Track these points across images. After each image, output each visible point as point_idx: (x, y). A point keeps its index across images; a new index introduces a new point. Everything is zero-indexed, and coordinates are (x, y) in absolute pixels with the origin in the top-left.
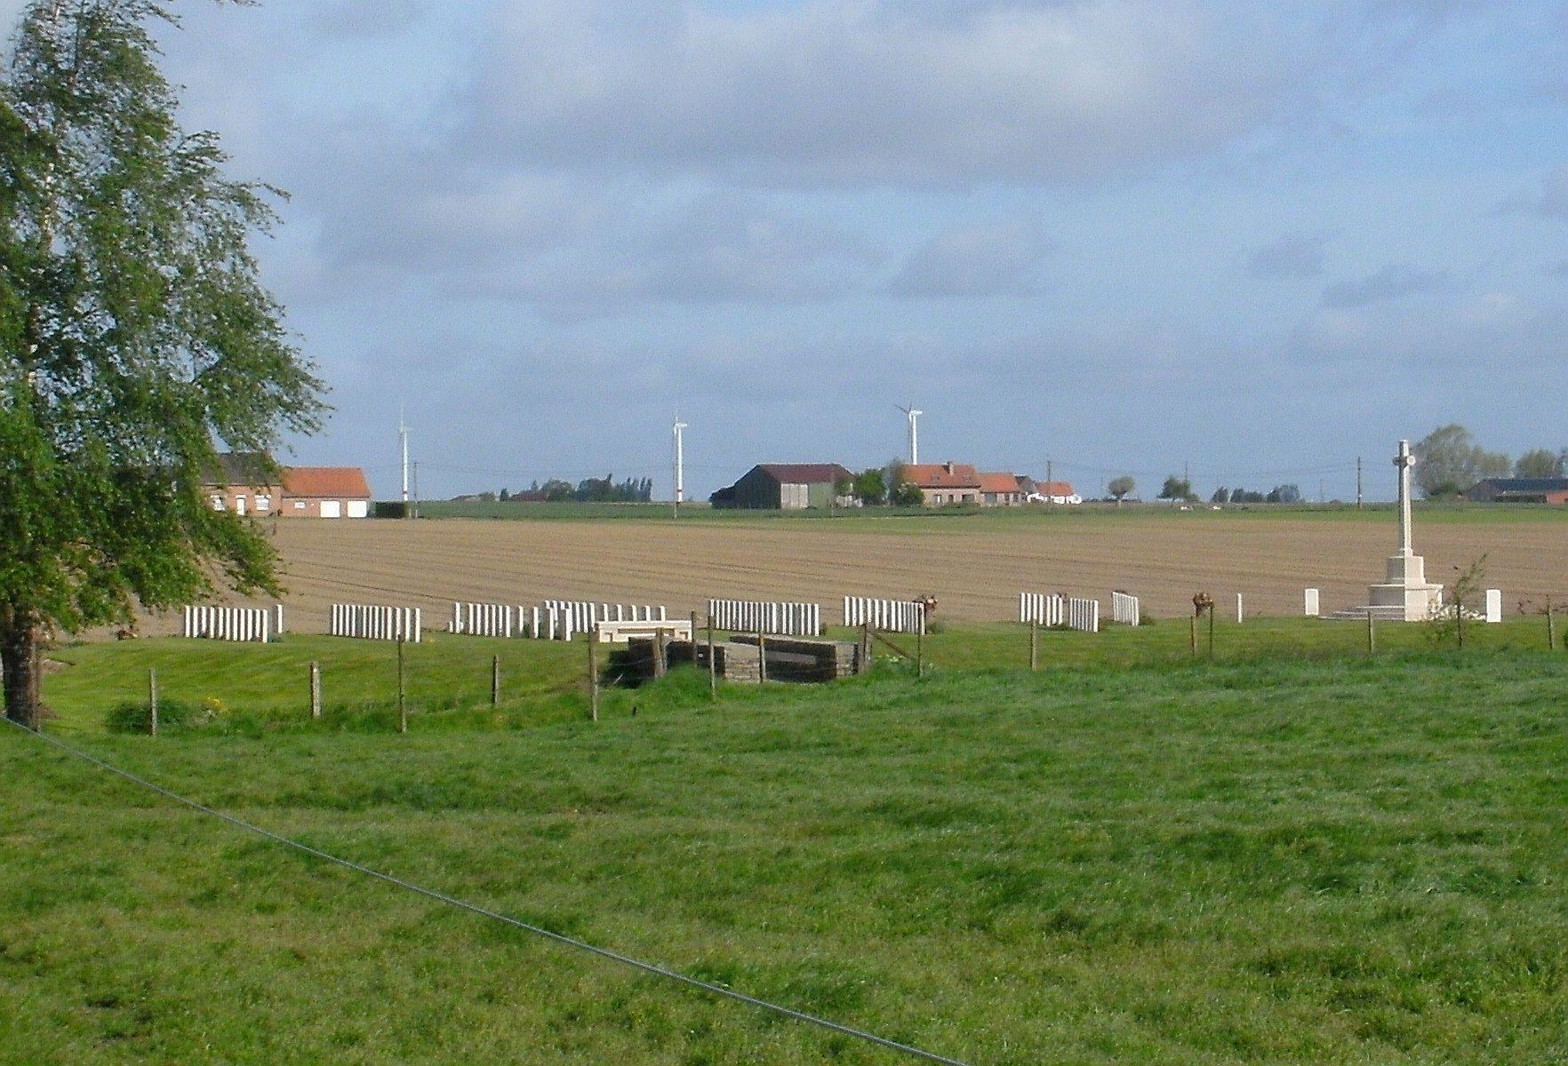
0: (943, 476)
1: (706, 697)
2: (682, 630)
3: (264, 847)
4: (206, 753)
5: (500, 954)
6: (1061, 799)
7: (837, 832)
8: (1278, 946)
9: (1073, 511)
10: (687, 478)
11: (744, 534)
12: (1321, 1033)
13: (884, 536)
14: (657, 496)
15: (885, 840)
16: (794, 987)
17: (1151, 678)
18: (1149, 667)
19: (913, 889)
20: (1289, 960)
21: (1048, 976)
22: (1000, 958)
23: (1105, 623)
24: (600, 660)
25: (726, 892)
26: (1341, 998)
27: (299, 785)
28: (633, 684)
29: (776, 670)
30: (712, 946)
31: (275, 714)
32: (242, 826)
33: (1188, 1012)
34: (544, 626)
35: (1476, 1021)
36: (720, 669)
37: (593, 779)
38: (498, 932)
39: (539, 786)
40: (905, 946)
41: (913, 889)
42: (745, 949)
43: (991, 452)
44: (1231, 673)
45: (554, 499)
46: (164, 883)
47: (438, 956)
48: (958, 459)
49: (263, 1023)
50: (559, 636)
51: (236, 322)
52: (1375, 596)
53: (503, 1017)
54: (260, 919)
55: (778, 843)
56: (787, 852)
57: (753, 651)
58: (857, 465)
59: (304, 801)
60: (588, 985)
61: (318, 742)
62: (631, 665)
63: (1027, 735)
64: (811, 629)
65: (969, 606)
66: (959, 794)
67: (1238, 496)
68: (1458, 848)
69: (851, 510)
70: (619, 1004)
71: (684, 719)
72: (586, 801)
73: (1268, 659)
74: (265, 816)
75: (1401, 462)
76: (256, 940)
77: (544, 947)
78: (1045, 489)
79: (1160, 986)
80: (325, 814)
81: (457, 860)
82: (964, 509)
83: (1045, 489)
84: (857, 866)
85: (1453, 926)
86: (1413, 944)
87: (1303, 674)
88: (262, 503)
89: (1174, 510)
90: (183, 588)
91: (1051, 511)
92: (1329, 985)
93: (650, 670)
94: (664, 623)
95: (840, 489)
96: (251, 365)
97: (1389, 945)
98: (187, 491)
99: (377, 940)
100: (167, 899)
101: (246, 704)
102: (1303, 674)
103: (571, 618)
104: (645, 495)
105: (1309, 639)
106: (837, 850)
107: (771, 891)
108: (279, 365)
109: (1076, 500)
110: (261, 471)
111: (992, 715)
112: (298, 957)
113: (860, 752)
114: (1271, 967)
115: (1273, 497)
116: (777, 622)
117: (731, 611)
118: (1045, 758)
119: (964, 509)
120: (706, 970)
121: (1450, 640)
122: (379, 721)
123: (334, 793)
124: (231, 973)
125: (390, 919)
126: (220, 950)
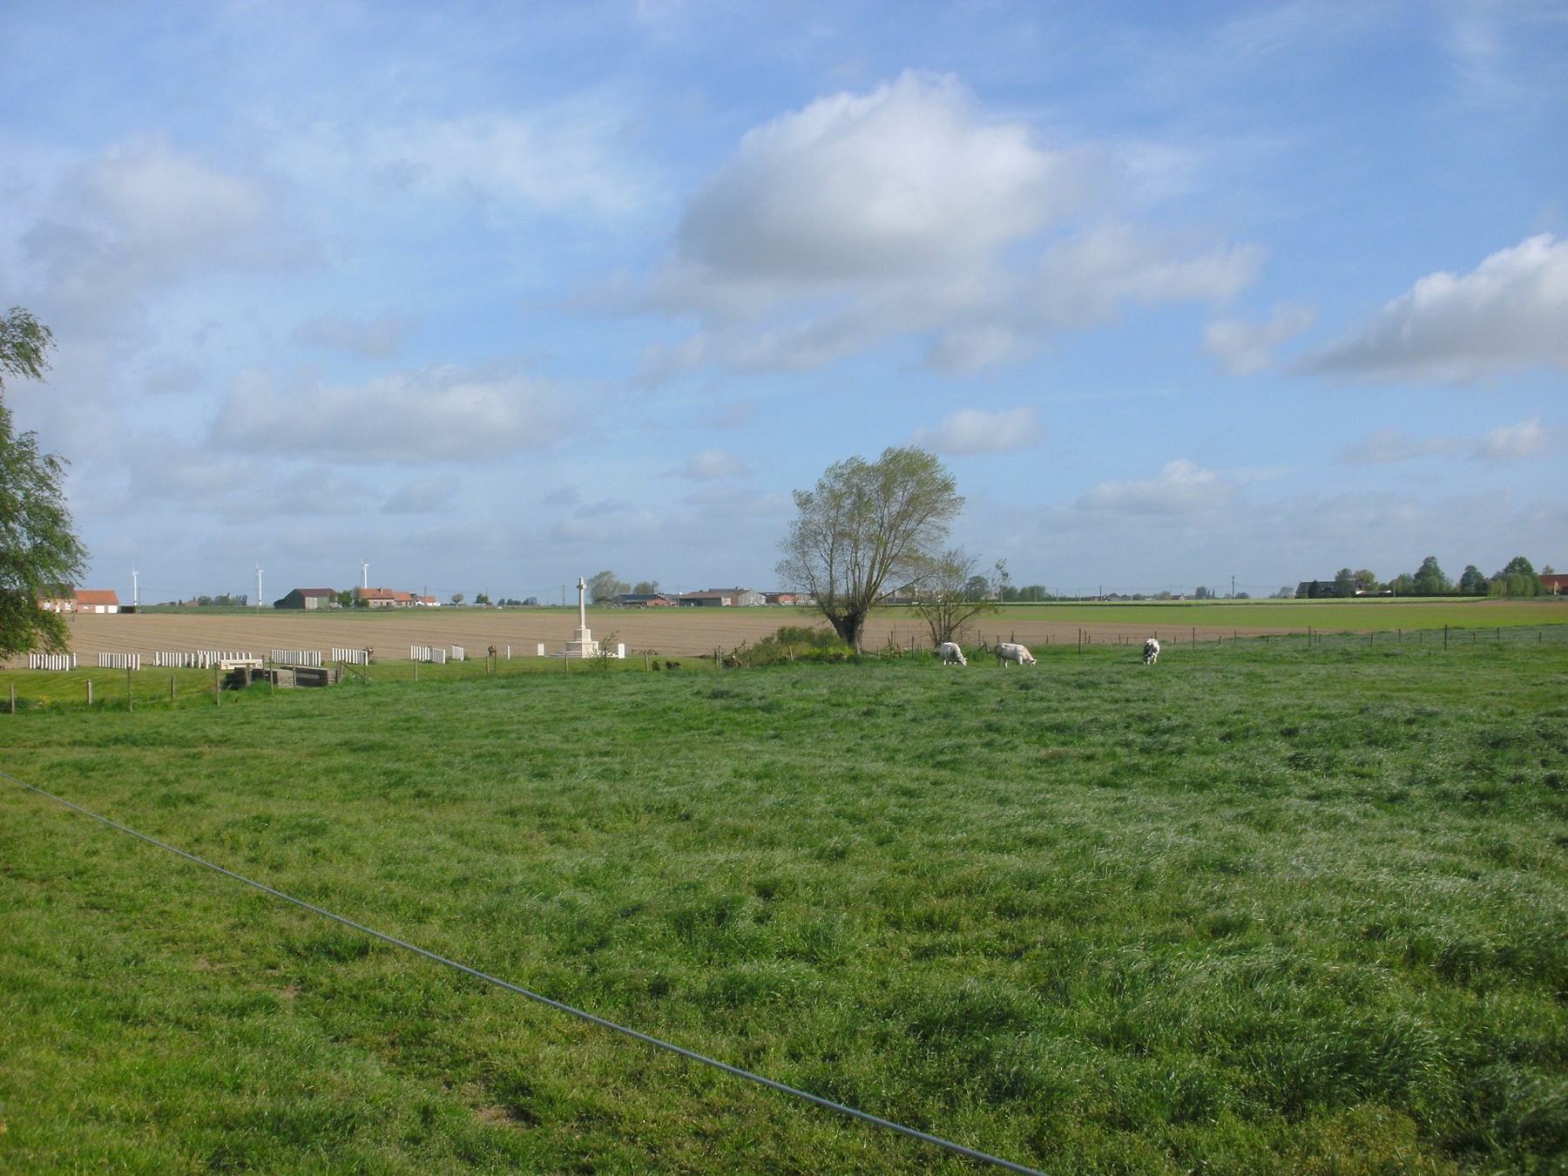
0: (378, 593)
2: (258, 664)
3: (60, 764)
4: (37, 722)
5: (166, 812)
6: (425, 739)
8: (516, 803)
9: (436, 609)
10: (263, 596)
11: (289, 619)
12: (533, 843)
13: (351, 621)
14: (250, 603)
16: (298, 825)
17: (469, 684)
18: (467, 679)
19: (354, 780)
20: (520, 810)
21: (413, 818)
22: (392, 810)
23: (449, 659)
24: (222, 677)
26: (542, 826)
27: (79, 736)
29: (301, 681)
30: (261, 807)
31: (72, 703)
32: (52, 755)
33: (473, 834)
35: (603, 836)
36: (276, 681)
37: (216, 731)
38: (166, 801)
39: (190, 735)
40: (350, 806)
41: (354, 780)
42: (280, 809)
43: (399, 583)
44: (503, 682)
45: (204, 605)
47: (138, 813)
49: (53, 846)
51: (49, 521)
52: (569, 647)
53: (165, 841)
55: (295, 759)
56: (299, 764)
57: (290, 673)
58: (340, 588)
59: (82, 743)
60: (205, 825)
62: (236, 680)
64: (317, 661)
65: (388, 652)
67: (510, 602)
68: (597, 759)
69: (333, 610)
70: (218, 834)
72: (210, 742)
73: (521, 677)
74: (62, 750)
75: (580, 587)
76: (53, 808)
78: (423, 599)
79: (462, 823)
81: (147, 769)
82: (387, 609)
83: (423, 599)
84: (329, 771)
85: (593, 794)
86: (574, 802)
87: (536, 682)
88: (68, 607)
89: (480, 609)
90: (28, 645)
91: (426, 610)
92: (538, 820)
93: (244, 682)
94: (251, 661)
95: (332, 600)
96: (54, 542)
97: (564, 803)
98: (33, 603)
99: (109, 806)
101: (58, 699)
102: (536, 682)
103: (207, 658)
104: (244, 603)
105: (539, 666)
106: (322, 763)
108: (67, 544)
109: (437, 604)
110: (65, 592)
114: (512, 813)
115: (526, 603)
117: (280, 655)
118: (418, 720)
119: (387, 609)
120: (258, 817)
121: (601, 667)
122: (120, 706)
123: (95, 740)
124: (39, 824)
125: (116, 797)
126: (35, 813)
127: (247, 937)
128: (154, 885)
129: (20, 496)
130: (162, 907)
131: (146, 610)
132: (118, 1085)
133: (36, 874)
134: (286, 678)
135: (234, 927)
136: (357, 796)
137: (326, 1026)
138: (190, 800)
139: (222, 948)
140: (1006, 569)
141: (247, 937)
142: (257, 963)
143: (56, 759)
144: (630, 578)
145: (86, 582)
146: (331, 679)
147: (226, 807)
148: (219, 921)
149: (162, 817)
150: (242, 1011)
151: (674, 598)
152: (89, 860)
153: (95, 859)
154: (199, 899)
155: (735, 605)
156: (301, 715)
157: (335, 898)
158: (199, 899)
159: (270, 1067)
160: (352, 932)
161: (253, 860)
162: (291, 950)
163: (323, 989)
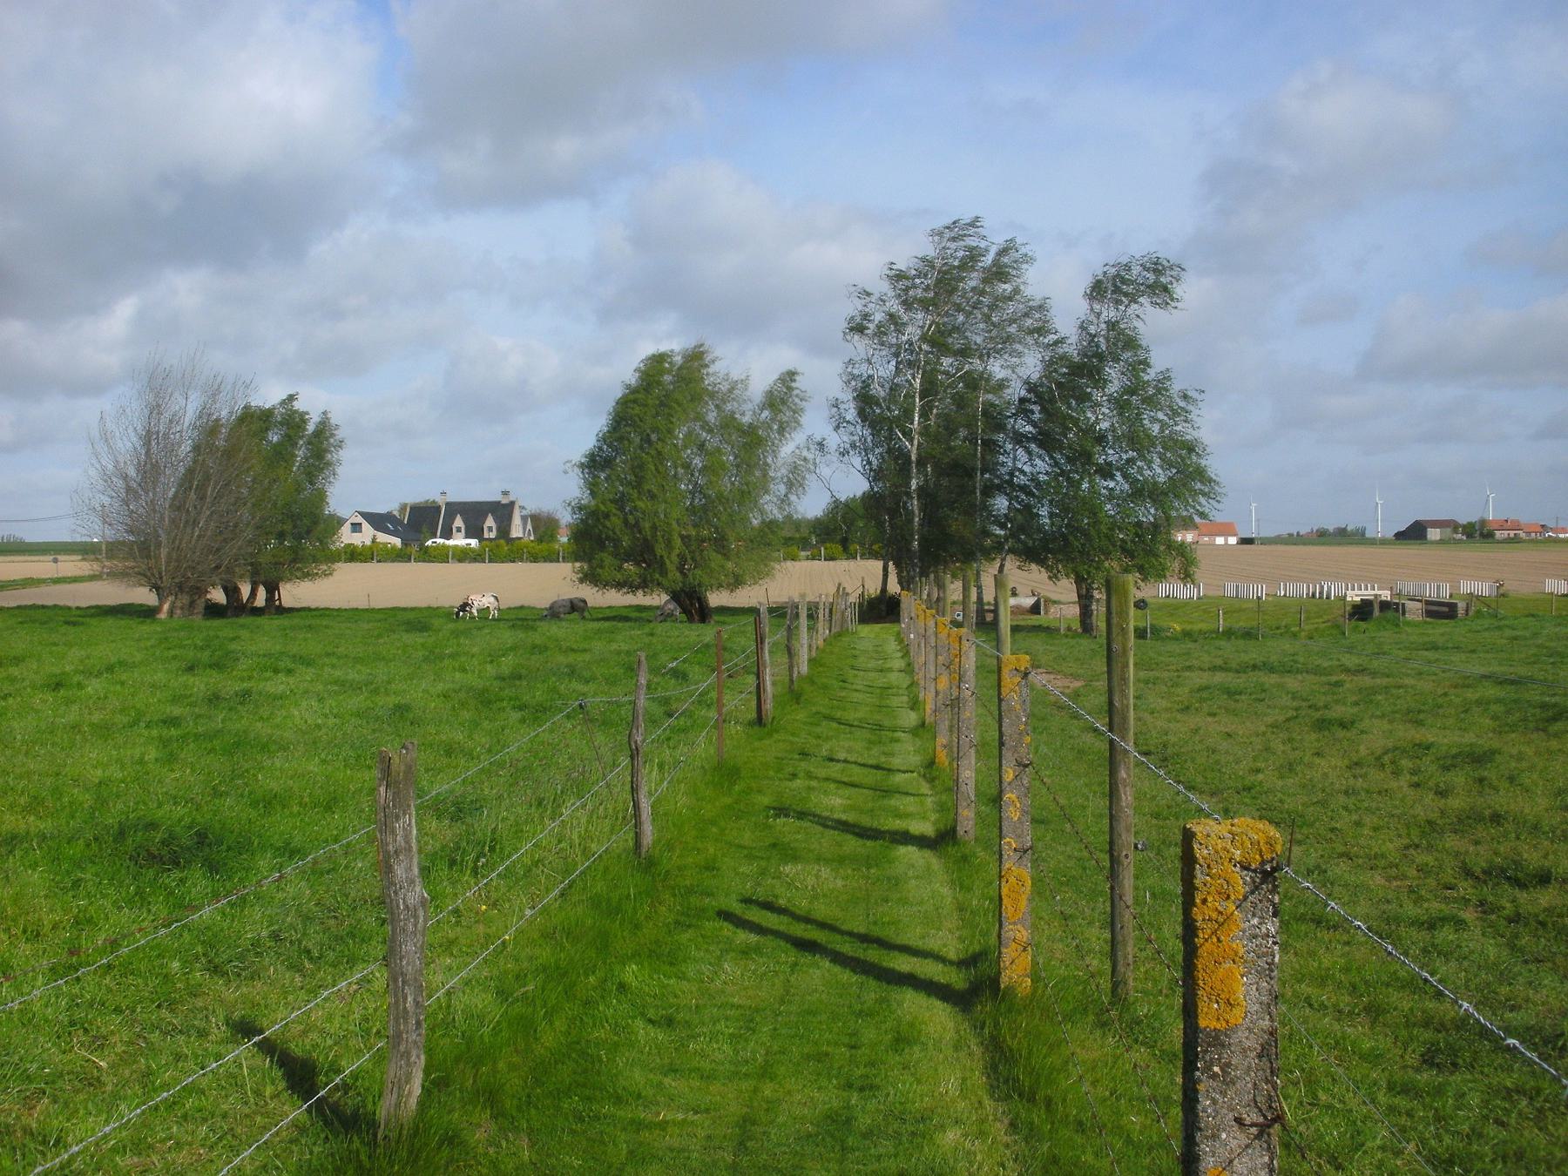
0: (1504, 525)
1: (1397, 625)
2: (1386, 595)
3: (1207, 688)
7: (1468, 686)
10: (1383, 526)
11: (1411, 551)
13: (1477, 553)
15: (1492, 691)
19: (1508, 712)
22: (1554, 744)
25: (1420, 712)
27: (1219, 662)
28: (1363, 620)
29: (1429, 614)
30: (1419, 735)
32: (1199, 679)
34: (1321, 593)
37: (1351, 661)
39: (1326, 664)
41: (1508, 712)
43: (1528, 514)
45: (1322, 537)
46: (1164, 703)
48: (1512, 517)
49: (1217, 762)
50: (1328, 597)
54: (1210, 719)
56: (1445, 694)
57: (1419, 605)
58: (1463, 520)
59: (1221, 669)
61: (1223, 643)
62: (1362, 611)
63: (1553, 644)
64: (1445, 594)
66: (1523, 671)
71: (1387, 636)
72: (1347, 671)
77: (1341, 733)
80: (1231, 674)
82: (1515, 540)
90: (1161, 576)
91: (1557, 541)
93: (1371, 613)
96: (1190, 475)
99: (1263, 728)
100: (1167, 710)
101: (1188, 627)
103: (1334, 589)
107: (1441, 711)
108: (1200, 474)
110: (1187, 524)
111: (1535, 635)
112: (1229, 735)
113: (1473, 651)
116: (1430, 592)
117: (1409, 587)
119: (1515, 540)
122: (1248, 635)
125: (1270, 720)
127: (1423, 858)
128: (1323, 803)
129: (1156, 428)
130: (1333, 824)
131: (1266, 541)
132: (1322, 980)
133: (1206, 788)
134: (1414, 610)
135: (1407, 847)
136: (1513, 728)
137: (1512, 947)
138: (1343, 725)
139: (1397, 866)
141: (1423, 858)
142: (1434, 883)
143: (1204, 682)
145: (1220, 512)
146: (1461, 612)
147: (1377, 735)
148: (1391, 841)
149: (1318, 740)
150: (1431, 925)
152: (1252, 778)
153: (1260, 776)
154: (1368, 820)
156: (1435, 648)
157: (1510, 827)
158: (1368, 820)
159: (1468, 980)
160: (1533, 858)
161: (1417, 785)
162: (1468, 873)
163: (1506, 912)
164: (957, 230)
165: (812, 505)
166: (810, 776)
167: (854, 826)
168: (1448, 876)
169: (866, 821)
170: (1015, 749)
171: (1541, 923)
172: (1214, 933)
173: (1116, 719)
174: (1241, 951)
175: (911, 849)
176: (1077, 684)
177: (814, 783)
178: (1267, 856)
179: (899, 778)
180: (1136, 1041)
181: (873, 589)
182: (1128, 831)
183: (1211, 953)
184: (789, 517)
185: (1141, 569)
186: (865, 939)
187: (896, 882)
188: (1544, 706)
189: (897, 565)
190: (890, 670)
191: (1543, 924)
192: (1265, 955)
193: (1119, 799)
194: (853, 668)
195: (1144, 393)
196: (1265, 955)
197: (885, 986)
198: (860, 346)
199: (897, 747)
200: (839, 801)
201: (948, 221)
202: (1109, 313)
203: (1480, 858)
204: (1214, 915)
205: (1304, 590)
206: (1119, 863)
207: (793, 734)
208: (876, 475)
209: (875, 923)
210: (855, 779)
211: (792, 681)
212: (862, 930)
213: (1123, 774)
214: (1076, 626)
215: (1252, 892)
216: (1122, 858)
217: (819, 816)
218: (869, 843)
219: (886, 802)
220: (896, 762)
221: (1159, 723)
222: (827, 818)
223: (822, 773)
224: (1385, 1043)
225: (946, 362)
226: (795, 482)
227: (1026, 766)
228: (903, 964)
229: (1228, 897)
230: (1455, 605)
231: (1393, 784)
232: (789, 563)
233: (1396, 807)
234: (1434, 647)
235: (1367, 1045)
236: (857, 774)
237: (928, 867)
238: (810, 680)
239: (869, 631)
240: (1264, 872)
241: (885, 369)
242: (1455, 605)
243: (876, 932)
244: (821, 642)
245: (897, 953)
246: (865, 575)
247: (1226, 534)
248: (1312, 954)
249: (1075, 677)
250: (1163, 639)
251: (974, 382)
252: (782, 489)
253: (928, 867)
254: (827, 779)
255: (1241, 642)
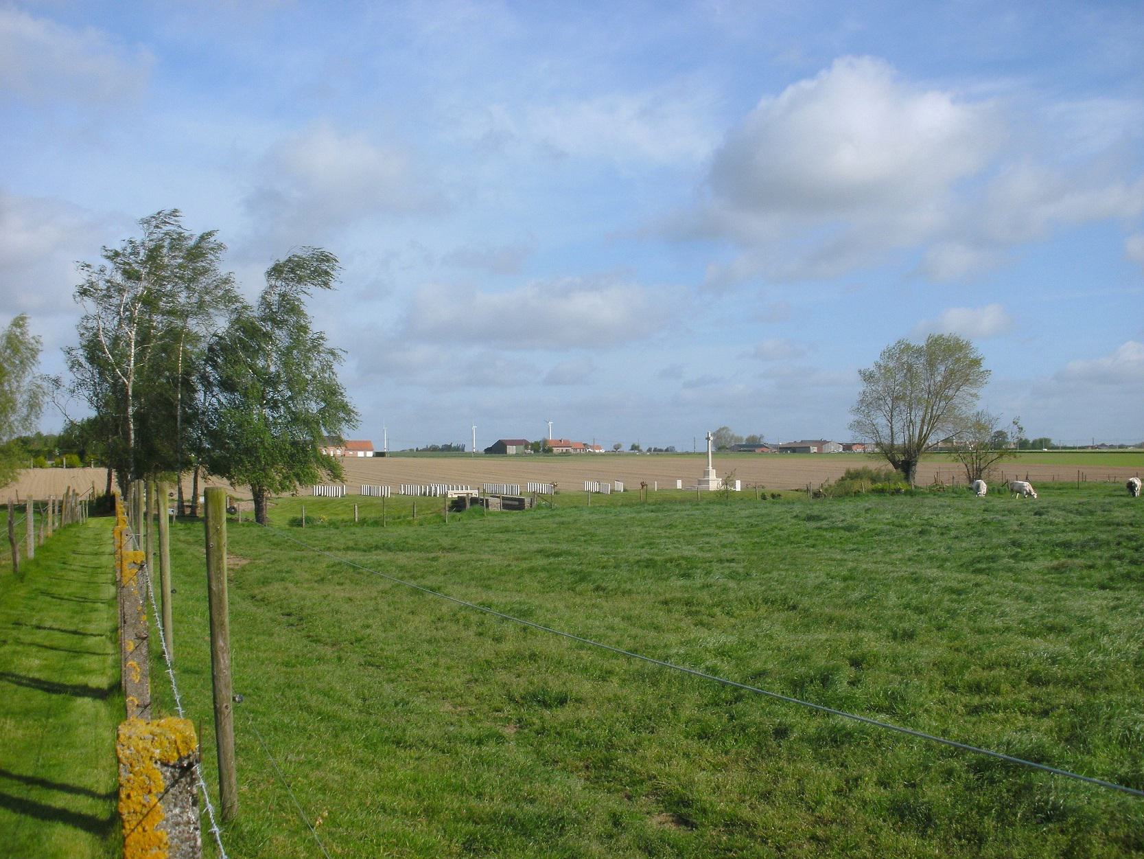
0: (559, 443)
2: (475, 493)
3: (339, 564)
10: (477, 444)
11: (495, 462)
13: (541, 463)
15: (541, 562)
22: (578, 600)
27: (351, 544)
29: (505, 506)
30: (485, 596)
37: (446, 542)
39: (429, 544)
43: (576, 435)
45: (433, 451)
46: (307, 576)
48: (564, 438)
49: (339, 621)
52: (700, 482)
57: (498, 500)
59: (353, 549)
61: (357, 530)
72: (444, 549)
82: (567, 454)
91: (595, 455)
96: (335, 407)
100: (308, 581)
101: (333, 517)
108: (344, 407)
110: (338, 442)
116: (505, 492)
119: (567, 454)
122: (377, 523)
125: (380, 588)
128: (411, 650)
130: (418, 666)
132: (396, 789)
133: (329, 640)
135: (469, 681)
139: (461, 696)
140: (1021, 424)
141: (479, 689)
144: (742, 432)
146: (527, 505)
147: (459, 595)
148: (459, 677)
151: (775, 447)
155: (820, 452)
160: (555, 687)
161: (480, 634)
162: (511, 699)
164: (158, 220)
165: (51, 424)
166: (18, 642)
167: (44, 682)
168: (497, 703)
169: (56, 678)
170: (134, 626)
171: (558, 733)
172: (140, 823)
173: (215, 601)
174: (166, 838)
175: (87, 700)
176: (245, 562)
177: (19, 648)
178: (184, 753)
179: (90, 641)
180: (240, 852)
181: (101, 490)
182: (227, 687)
183: (138, 842)
184: (39, 435)
185: (297, 476)
186: (31, 781)
187: (68, 729)
188: (573, 573)
189: (119, 471)
190: (103, 553)
191: (559, 734)
192: (188, 839)
193: (218, 662)
194: (74, 552)
195: (304, 344)
196: (188, 839)
197: (39, 821)
198: (90, 306)
199: (94, 615)
200: (37, 662)
201: (154, 212)
202: (281, 286)
203: (520, 686)
204: (138, 808)
205: (418, 490)
206: (221, 713)
207: (11, 608)
208: (99, 401)
209: (43, 766)
210: (55, 643)
211: (15, 564)
212: (30, 773)
213: (221, 643)
214: (252, 517)
215: (173, 786)
216: (223, 708)
217: (16, 676)
218: (54, 696)
219: (75, 661)
220: (91, 628)
221: (299, 592)
222: (24, 678)
223: (28, 639)
224: (437, 838)
225: (157, 318)
226: (34, 405)
227: (144, 639)
228: (60, 801)
229: (150, 792)
230: (522, 501)
231: (464, 634)
232: (38, 470)
233: (464, 651)
234: (507, 531)
235: (421, 841)
236: (58, 639)
237: (97, 715)
238: (36, 562)
239: (94, 522)
240: (182, 767)
241: (110, 323)
242: (522, 501)
243: (42, 774)
244: (50, 532)
245: (55, 792)
246: (92, 479)
247: (365, 449)
248: (390, 769)
249: (244, 556)
250: (314, 527)
251: (174, 335)
252: (25, 411)
253: (97, 715)
254: (31, 644)
255: (370, 529)
